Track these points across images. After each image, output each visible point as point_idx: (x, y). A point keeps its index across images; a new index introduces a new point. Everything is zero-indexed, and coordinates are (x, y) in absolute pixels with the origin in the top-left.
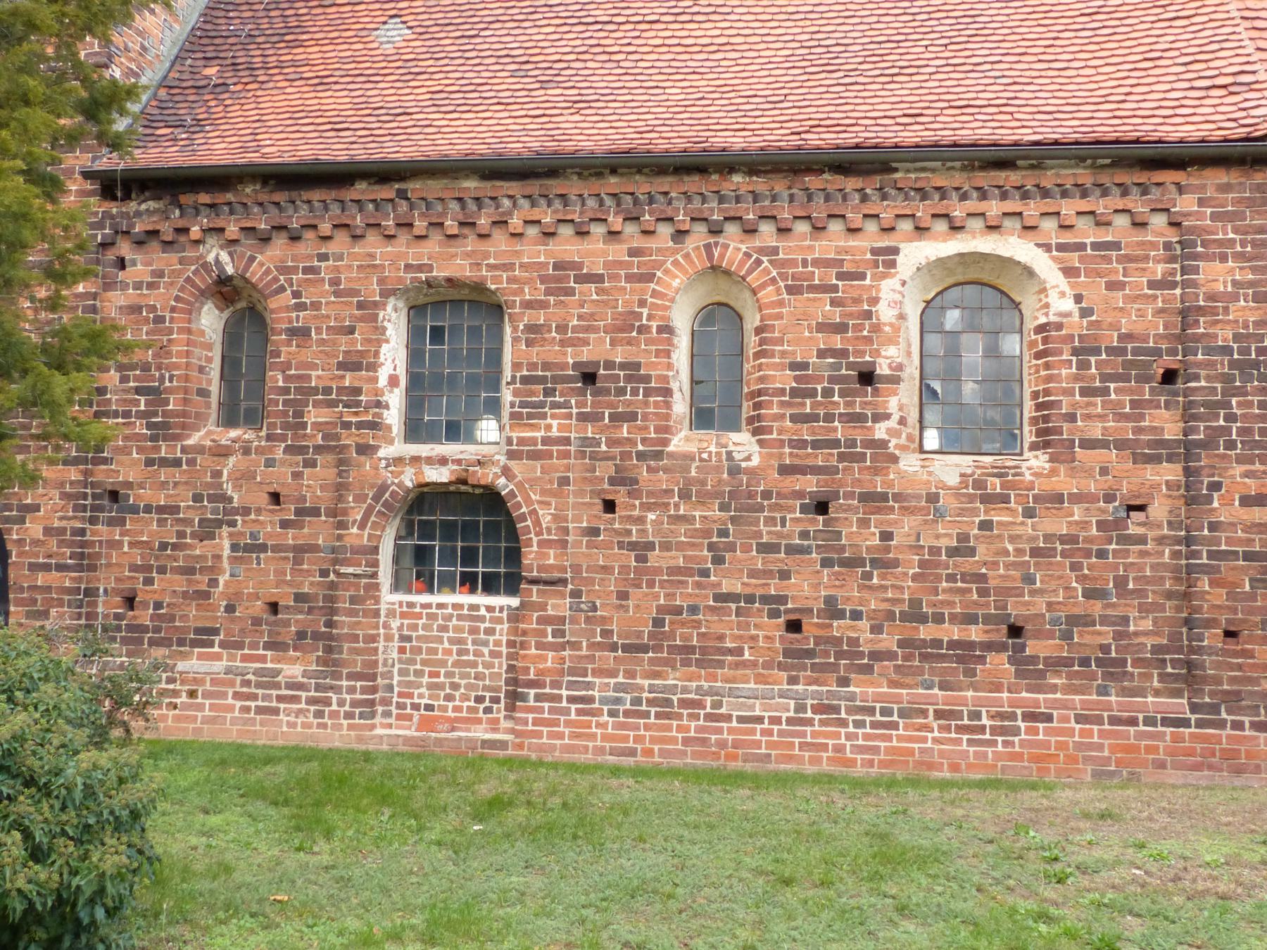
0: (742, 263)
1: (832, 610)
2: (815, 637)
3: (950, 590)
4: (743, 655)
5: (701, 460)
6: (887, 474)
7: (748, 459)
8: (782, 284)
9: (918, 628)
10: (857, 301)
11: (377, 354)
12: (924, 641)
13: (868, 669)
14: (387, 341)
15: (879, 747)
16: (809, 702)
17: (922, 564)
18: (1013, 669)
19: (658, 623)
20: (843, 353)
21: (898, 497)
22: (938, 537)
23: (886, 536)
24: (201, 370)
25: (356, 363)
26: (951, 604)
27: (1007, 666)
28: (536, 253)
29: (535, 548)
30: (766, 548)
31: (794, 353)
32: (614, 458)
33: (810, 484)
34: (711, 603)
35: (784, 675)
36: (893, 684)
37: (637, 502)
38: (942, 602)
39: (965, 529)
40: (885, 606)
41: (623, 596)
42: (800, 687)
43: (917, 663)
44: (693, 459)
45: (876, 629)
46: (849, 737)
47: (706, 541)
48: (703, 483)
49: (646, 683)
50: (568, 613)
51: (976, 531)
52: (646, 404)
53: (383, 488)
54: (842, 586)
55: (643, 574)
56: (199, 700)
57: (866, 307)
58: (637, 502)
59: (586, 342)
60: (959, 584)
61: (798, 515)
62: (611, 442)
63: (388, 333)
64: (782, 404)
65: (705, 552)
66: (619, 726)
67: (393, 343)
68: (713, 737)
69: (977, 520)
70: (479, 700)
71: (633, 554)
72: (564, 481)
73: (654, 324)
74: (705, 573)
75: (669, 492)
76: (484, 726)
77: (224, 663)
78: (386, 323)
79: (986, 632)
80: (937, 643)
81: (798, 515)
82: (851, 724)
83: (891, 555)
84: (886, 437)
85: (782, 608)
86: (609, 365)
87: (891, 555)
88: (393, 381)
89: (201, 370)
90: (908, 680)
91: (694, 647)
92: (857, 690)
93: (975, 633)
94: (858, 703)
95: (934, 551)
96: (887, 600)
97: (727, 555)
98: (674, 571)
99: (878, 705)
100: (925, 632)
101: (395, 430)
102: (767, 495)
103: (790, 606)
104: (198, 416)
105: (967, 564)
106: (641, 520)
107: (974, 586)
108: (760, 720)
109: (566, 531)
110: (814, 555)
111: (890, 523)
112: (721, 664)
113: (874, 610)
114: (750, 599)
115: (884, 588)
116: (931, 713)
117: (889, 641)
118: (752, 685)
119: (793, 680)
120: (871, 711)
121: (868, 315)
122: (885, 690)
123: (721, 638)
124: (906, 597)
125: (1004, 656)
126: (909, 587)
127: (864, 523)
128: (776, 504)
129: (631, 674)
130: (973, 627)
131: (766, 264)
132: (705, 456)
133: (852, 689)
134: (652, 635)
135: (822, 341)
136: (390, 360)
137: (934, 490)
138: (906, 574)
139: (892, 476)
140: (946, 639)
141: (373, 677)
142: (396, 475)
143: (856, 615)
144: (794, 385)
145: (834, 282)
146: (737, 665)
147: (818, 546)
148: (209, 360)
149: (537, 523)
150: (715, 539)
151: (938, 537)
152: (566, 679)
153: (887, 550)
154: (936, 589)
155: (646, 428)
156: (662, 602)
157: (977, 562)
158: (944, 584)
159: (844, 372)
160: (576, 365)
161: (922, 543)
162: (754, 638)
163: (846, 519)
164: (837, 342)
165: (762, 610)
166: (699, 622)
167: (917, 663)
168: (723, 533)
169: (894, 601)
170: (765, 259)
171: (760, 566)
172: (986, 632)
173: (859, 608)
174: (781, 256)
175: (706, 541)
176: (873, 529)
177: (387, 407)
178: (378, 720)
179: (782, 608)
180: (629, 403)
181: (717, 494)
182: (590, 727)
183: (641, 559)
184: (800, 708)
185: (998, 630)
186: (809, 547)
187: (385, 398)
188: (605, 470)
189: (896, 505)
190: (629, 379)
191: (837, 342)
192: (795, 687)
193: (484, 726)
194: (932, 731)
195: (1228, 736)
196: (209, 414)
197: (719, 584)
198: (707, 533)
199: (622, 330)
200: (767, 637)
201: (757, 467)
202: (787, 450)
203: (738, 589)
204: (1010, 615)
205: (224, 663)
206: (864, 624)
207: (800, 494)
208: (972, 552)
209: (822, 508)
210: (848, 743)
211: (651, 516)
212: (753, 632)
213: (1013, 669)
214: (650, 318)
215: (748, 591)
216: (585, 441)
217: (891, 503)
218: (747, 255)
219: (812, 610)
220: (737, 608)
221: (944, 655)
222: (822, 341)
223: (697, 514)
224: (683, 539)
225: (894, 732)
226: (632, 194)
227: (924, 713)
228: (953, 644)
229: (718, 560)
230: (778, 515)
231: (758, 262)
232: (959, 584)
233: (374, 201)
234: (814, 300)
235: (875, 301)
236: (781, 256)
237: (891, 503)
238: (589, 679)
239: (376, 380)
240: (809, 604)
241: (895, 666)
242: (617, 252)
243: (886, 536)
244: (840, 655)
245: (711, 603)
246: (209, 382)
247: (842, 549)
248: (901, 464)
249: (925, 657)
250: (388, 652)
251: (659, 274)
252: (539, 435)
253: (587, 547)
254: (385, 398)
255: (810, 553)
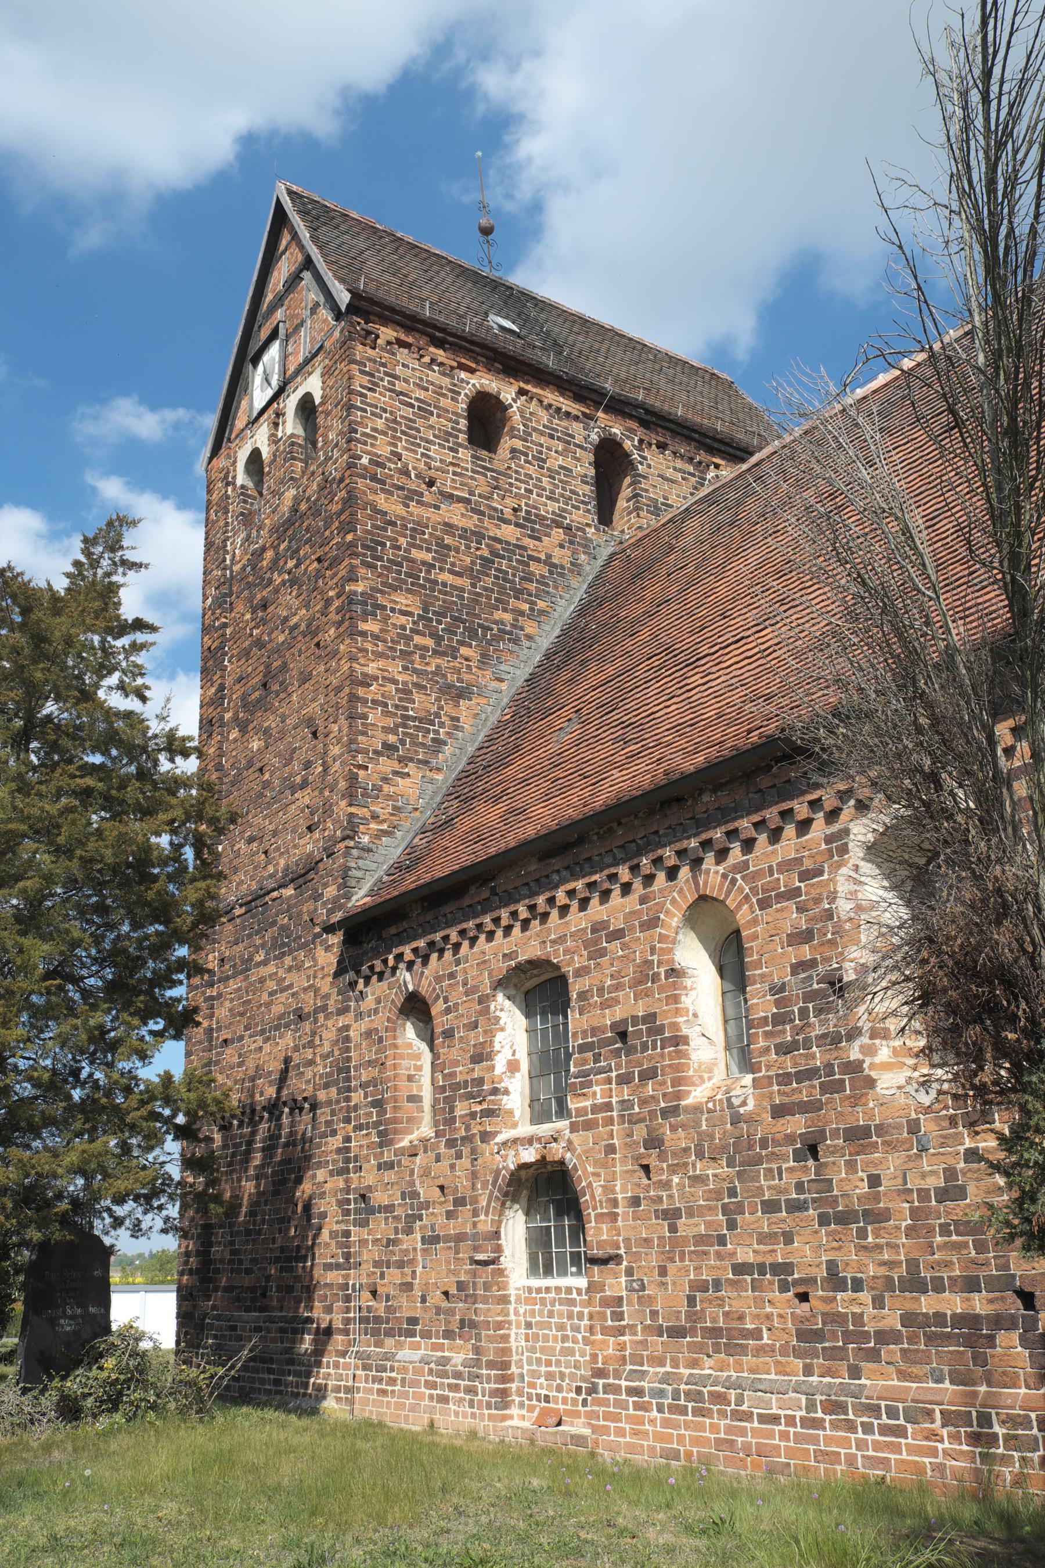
0: (721, 885)
1: (835, 1280)
2: (823, 1314)
3: (944, 1246)
4: (761, 1339)
5: (709, 1111)
6: (865, 1104)
7: (744, 1103)
8: (754, 900)
9: (918, 1299)
10: (818, 901)
11: (492, 1042)
12: (926, 1315)
13: (873, 1356)
14: (502, 1029)
15: (888, 1460)
16: (819, 1398)
17: (914, 1213)
18: (1027, 1352)
19: (691, 1301)
20: (812, 964)
21: (881, 1129)
22: (923, 1176)
23: (874, 1181)
24: (410, 1078)
25: (482, 1056)
26: (948, 1264)
27: (1020, 1349)
28: (578, 920)
29: (593, 1224)
30: (770, 1207)
31: (771, 974)
32: (643, 1120)
33: (797, 1124)
34: (731, 1276)
35: (799, 1363)
36: (903, 1375)
37: (665, 1165)
38: (938, 1263)
39: (951, 1161)
40: (883, 1271)
41: (663, 1271)
42: (815, 1379)
43: (923, 1347)
44: (702, 1112)
45: (878, 1302)
46: (861, 1445)
47: (720, 1203)
48: (712, 1137)
49: (687, 1372)
50: (624, 1293)
51: (962, 1165)
52: (662, 1056)
53: (497, 1172)
54: (840, 1248)
55: (673, 1249)
56: (646, 1399)
57: (827, 906)
58: (665, 1165)
59: (616, 1001)
60: (954, 1238)
61: (792, 1163)
62: (643, 1102)
63: (502, 1022)
64: (767, 1034)
65: (721, 1217)
66: (666, 1423)
67: (509, 1030)
68: (740, 1439)
69: (961, 1149)
70: (578, 1390)
71: (666, 1223)
72: (611, 1149)
73: (662, 970)
74: (722, 1241)
75: (686, 1150)
76: (583, 1420)
77: (422, 1352)
78: (498, 1013)
79: (991, 1301)
80: (939, 1318)
81: (792, 1163)
82: (860, 1429)
83: (881, 1205)
84: (861, 1057)
85: (790, 1279)
86: (635, 1018)
87: (881, 1205)
88: (513, 1066)
89: (410, 1078)
90: (915, 1370)
91: (721, 1329)
92: (868, 1382)
93: (980, 1304)
94: (863, 1400)
95: (923, 1194)
96: (883, 1263)
97: (739, 1218)
98: (700, 1239)
99: (883, 1403)
100: (927, 1304)
101: (517, 1114)
102: (764, 1143)
103: (796, 1276)
104: (410, 1120)
105: (957, 1209)
106: (667, 1185)
107: (970, 1239)
108: (775, 1419)
109: (615, 1203)
110: (811, 1211)
111: (876, 1164)
112: (743, 1350)
113: (874, 1277)
114: (762, 1269)
115: (878, 1247)
116: (938, 1415)
117: (892, 1320)
118: (773, 1377)
119: (808, 1371)
120: (875, 1410)
121: (829, 915)
122: (895, 1382)
123: (741, 1318)
124: (903, 1258)
125: (1015, 1336)
126: (903, 1245)
127: (851, 1166)
128: (773, 1153)
129: (675, 1364)
130: (976, 1296)
131: (740, 881)
132: (710, 1105)
133: (863, 1381)
134: (689, 1316)
135: (793, 955)
136: (507, 1047)
137: (914, 1116)
138: (898, 1228)
139: (871, 1105)
140: (949, 1313)
141: (506, 1366)
142: (505, 1158)
143: (858, 1285)
144: (775, 1010)
145: (798, 884)
146: (760, 1351)
147: (814, 1200)
148: (419, 1068)
149: (593, 1196)
150: (726, 1200)
151: (923, 1176)
152: (629, 1367)
153: (877, 1198)
154: (930, 1245)
155: (664, 1083)
156: (692, 1277)
157: (969, 1206)
158: (939, 1239)
159: (815, 986)
160: (614, 1025)
161: (909, 1186)
162: (769, 1317)
163: (834, 1163)
164: (806, 952)
165: (771, 1283)
166: (722, 1299)
167: (923, 1347)
168: (732, 1192)
169: (891, 1264)
170: (738, 876)
171: (766, 1230)
172: (991, 1301)
173: (859, 1275)
174: (752, 869)
175: (720, 1203)
176: (860, 1174)
177: (506, 1092)
178: (514, 1411)
179: (790, 1279)
180: (651, 1058)
181: (724, 1148)
182: (643, 1424)
183: (673, 1229)
184: (811, 1407)
185: (1003, 1299)
186: (805, 1201)
187: (503, 1085)
188: (640, 1132)
189: (879, 1140)
190: (651, 1032)
191: (806, 952)
192: (811, 1379)
193: (583, 1420)
194: (942, 1441)
195: (874, 1442)
196: (422, 1118)
197: (735, 1253)
198: (717, 1195)
199: (640, 983)
200: (780, 1316)
201: (751, 1113)
202: (776, 1088)
203: (751, 1258)
204: (1013, 1276)
205: (422, 1352)
206: (865, 1296)
207: (790, 1139)
208: (961, 1193)
209: (813, 1150)
210: (859, 1453)
211: (676, 1180)
212: (768, 1310)
213: (1027, 1352)
214: (660, 963)
215: (760, 1259)
216: (626, 1104)
217: (874, 1138)
218: (724, 876)
219: (816, 1281)
220: (753, 1280)
221: (948, 1336)
222: (793, 955)
223: (710, 1172)
224: (702, 1202)
225: (903, 1441)
226: (634, 841)
227: (930, 1413)
228: (960, 1320)
229: (732, 1225)
230: (775, 1166)
231: (734, 881)
232: (954, 1238)
233: (479, 903)
234: (782, 910)
235: (833, 897)
236: (752, 869)
237: (874, 1138)
238: (645, 1368)
239: (492, 1068)
240: (813, 1272)
241: (901, 1350)
242: (631, 902)
243: (874, 1181)
244: (848, 1338)
245: (731, 1276)
246: (420, 1088)
247: (835, 1201)
248: (880, 1085)
249: (930, 1339)
250: (517, 1339)
251: (662, 916)
252: (588, 1103)
253: (634, 1219)
254: (503, 1085)
255: (807, 1209)
